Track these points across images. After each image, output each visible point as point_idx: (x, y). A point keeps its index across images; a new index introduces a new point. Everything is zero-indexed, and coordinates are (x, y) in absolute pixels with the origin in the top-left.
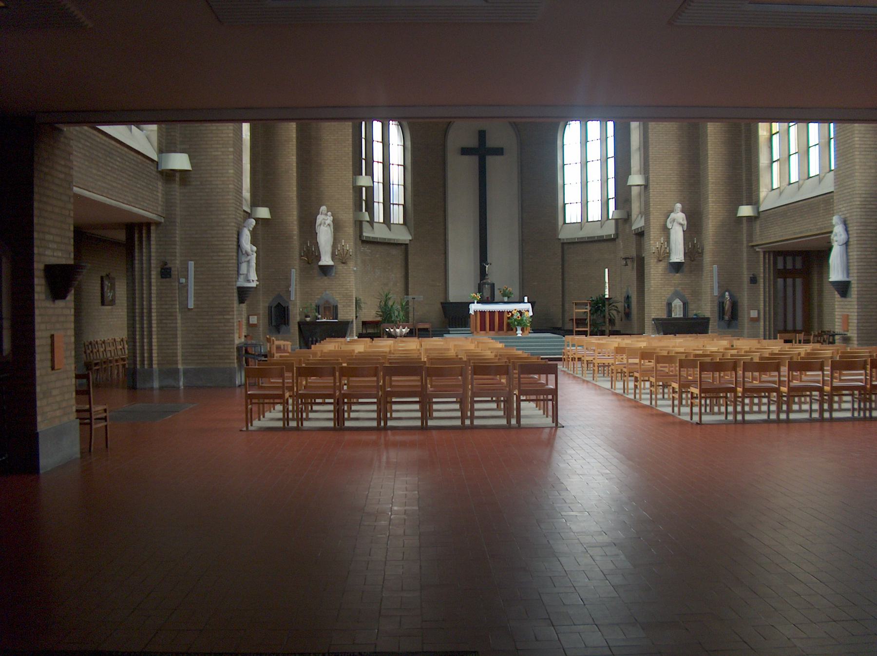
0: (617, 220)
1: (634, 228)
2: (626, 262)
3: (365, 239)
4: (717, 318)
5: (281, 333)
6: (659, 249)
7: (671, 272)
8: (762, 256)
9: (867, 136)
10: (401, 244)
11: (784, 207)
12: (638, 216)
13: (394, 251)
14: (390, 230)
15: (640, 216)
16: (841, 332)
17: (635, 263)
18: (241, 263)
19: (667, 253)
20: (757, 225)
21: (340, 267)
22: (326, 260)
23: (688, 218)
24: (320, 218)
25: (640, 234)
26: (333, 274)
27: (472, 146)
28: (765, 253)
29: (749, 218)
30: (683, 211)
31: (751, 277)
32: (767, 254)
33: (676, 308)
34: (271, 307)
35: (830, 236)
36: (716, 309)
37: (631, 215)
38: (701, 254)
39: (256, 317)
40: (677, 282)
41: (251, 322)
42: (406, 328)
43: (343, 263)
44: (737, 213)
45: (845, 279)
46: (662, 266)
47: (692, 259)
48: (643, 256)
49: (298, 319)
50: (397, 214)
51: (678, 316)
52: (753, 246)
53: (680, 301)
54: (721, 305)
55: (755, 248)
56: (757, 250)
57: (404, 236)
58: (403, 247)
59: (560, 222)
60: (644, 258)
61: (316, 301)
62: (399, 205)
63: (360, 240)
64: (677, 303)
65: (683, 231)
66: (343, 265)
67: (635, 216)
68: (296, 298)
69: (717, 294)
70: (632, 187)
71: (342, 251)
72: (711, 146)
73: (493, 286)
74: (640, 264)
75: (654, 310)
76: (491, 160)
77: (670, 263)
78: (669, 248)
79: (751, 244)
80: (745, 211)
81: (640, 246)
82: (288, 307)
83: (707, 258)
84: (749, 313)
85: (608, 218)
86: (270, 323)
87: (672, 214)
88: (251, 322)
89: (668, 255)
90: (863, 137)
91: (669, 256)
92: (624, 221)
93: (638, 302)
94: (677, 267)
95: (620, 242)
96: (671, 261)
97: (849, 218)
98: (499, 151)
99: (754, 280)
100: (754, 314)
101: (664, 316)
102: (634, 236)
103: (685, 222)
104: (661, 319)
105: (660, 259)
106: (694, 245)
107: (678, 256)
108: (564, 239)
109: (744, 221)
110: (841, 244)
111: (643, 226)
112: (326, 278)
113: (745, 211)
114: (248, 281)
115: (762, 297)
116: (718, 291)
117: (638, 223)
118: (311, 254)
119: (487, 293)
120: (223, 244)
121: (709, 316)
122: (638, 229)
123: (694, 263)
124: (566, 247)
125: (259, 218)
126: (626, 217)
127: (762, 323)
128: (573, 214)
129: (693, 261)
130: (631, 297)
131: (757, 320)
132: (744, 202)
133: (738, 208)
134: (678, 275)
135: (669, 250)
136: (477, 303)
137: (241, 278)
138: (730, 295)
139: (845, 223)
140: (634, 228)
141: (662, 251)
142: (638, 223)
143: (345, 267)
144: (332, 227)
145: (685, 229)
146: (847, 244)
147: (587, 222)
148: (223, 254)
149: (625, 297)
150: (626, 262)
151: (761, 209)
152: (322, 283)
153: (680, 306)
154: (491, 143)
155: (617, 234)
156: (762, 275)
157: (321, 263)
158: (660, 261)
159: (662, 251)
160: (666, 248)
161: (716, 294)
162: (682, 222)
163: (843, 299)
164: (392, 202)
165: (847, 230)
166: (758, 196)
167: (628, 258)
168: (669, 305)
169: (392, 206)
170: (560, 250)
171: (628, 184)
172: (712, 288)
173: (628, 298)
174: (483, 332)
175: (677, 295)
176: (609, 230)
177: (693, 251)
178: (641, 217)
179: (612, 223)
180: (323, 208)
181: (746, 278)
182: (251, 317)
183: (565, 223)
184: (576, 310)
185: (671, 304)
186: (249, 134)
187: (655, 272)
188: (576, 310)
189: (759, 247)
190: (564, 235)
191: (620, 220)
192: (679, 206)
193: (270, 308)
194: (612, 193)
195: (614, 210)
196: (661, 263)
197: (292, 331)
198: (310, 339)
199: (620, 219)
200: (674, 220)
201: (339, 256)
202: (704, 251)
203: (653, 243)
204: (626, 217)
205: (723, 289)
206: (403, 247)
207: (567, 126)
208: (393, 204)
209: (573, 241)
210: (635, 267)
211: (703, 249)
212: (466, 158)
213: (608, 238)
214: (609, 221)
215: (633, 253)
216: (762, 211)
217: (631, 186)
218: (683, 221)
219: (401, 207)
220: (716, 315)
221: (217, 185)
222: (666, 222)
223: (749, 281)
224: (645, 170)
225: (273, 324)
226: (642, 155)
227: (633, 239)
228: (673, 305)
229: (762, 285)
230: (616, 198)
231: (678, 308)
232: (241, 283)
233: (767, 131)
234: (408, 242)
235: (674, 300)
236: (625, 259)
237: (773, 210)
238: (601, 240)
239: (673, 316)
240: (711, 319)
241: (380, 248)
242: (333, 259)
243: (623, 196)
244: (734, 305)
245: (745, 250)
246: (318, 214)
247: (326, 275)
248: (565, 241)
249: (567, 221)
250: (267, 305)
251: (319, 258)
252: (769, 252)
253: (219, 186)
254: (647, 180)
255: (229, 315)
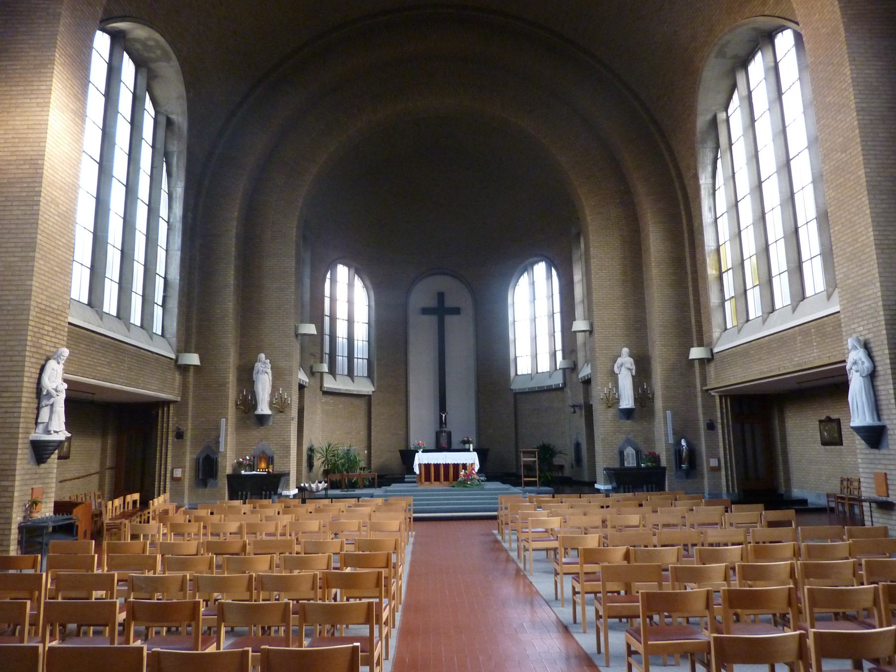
0: (564, 370)
1: (580, 376)
2: (574, 410)
3: (325, 390)
4: (674, 468)
5: (208, 487)
6: (608, 395)
7: (621, 418)
8: (718, 400)
9: (888, 228)
10: (365, 396)
11: (746, 345)
12: (584, 365)
13: (357, 402)
14: (152, 340)
15: (586, 364)
16: (874, 496)
17: (583, 410)
18: (41, 408)
19: (617, 399)
20: (711, 369)
21: (279, 416)
22: (264, 408)
23: (637, 362)
24: (258, 366)
25: (587, 382)
26: (271, 424)
27: (146, 82)
28: (721, 397)
29: (701, 361)
30: (630, 356)
31: (707, 423)
32: (724, 398)
33: (628, 456)
34: (199, 459)
35: (845, 366)
36: (673, 458)
37: (577, 365)
38: (652, 399)
39: (180, 470)
40: (627, 429)
41: (175, 476)
42: (323, 482)
43: (282, 412)
44: (688, 356)
45: (877, 423)
46: (612, 412)
47: (643, 405)
48: (591, 403)
49: (229, 471)
50: (361, 366)
51: (631, 465)
52: (707, 390)
53: (633, 450)
54: (678, 452)
55: (709, 392)
56: (713, 394)
57: (366, 388)
58: (366, 398)
59: (512, 374)
60: (592, 405)
61: (252, 453)
62: (363, 359)
63: (321, 390)
64: (630, 451)
65: (632, 376)
66: (281, 414)
67: (581, 365)
68: (226, 449)
69: (672, 442)
70: (577, 333)
71: (280, 399)
72: (657, 289)
73: (449, 434)
74: (589, 411)
75: (604, 460)
76: (450, 320)
77: (620, 409)
78: (618, 394)
79: (705, 388)
80: (696, 353)
81: (587, 394)
82: (216, 459)
83: (659, 404)
84: (708, 462)
85: (556, 369)
86: (197, 476)
87: (619, 359)
88: (175, 476)
89: (618, 401)
90: (885, 230)
91: (618, 402)
92: (571, 369)
93: (588, 449)
94: (628, 414)
95: (568, 390)
96: (620, 407)
97: (872, 340)
98: (456, 311)
99: (711, 426)
100: (714, 463)
101: (617, 465)
102: (581, 384)
103: (634, 367)
104: (614, 470)
105: (609, 405)
106: (644, 391)
107: (627, 401)
108: (515, 390)
109: (697, 364)
110: (864, 375)
111: (590, 374)
112: (262, 427)
113: (696, 353)
114: (48, 432)
115: (721, 444)
116: (673, 438)
117: (585, 371)
118: (248, 404)
119: (444, 442)
120: (9, 381)
121: (665, 466)
122: (584, 377)
123: (645, 409)
124: (518, 396)
125: (190, 365)
126: (573, 367)
127: (723, 472)
128: (524, 367)
129: (643, 407)
130: (580, 444)
131: (717, 469)
132: (695, 344)
133: (690, 349)
134: (628, 421)
135: (618, 396)
136: (423, 452)
137: (41, 427)
138: (687, 442)
139: (866, 346)
140: (580, 376)
141: (611, 397)
142: (585, 371)
143: (283, 416)
144: (270, 375)
145: (634, 374)
146: (872, 376)
147: (537, 373)
148: (8, 394)
149: (574, 444)
150: (574, 410)
151: (716, 350)
152: (257, 433)
153: (633, 456)
154: (449, 303)
155: (565, 384)
156: (719, 421)
157: (257, 412)
158: (610, 407)
159: (611, 397)
160: (615, 394)
161: (671, 441)
162: (631, 367)
163: (875, 451)
164: (356, 356)
165: (870, 355)
166: (711, 337)
167: (577, 406)
168: (621, 453)
169: (356, 360)
170: (512, 400)
171: (573, 330)
172: (667, 435)
173: (578, 446)
174: (427, 483)
175: (629, 442)
176: (558, 380)
177: (643, 398)
178: (587, 365)
179: (560, 374)
180: (262, 356)
181: (702, 425)
182: (174, 470)
183: (516, 374)
184: (524, 459)
185: (623, 452)
186: (179, 278)
187: (603, 419)
188: (524, 459)
189: (715, 391)
190: (516, 386)
191: (567, 370)
192: (625, 351)
193: (197, 461)
194: (559, 346)
195: (561, 360)
196: (610, 409)
197: (220, 484)
198: (240, 493)
199: (567, 368)
200: (622, 365)
201: (279, 406)
202: (655, 396)
203: (599, 391)
204: (573, 367)
205: (678, 436)
206: (366, 398)
207: (517, 287)
208: (358, 358)
209: (525, 391)
210: (583, 413)
211: (653, 395)
212: (426, 318)
213: (557, 387)
214: (557, 372)
215: (581, 400)
216: (717, 353)
217: (575, 332)
218: (631, 365)
219: (365, 361)
220: (673, 463)
221: (9, 300)
222: (614, 367)
223: (184, 435)
224: (589, 316)
225: (200, 477)
226: (585, 285)
227: (580, 389)
228: (625, 454)
229: (720, 431)
230: (563, 350)
231: (631, 457)
232: (39, 435)
233: (716, 270)
234: (371, 393)
235: (626, 448)
236: (574, 406)
237: (731, 350)
238: (550, 390)
239: (626, 464)
240: (668, 468)
241: (343, 399)
242: (271, 408)
243: (569, 348)
244: (693, 453)
245: (699, 394)
246: (256, 362)
247: (262, 426)
248: (517, 391)
249: (519, 373)
250: (195, 456)
251: (255, 407)
252: (726, 396)
253: (12, 303)
254: (591, 325)
255: (8, 481)
